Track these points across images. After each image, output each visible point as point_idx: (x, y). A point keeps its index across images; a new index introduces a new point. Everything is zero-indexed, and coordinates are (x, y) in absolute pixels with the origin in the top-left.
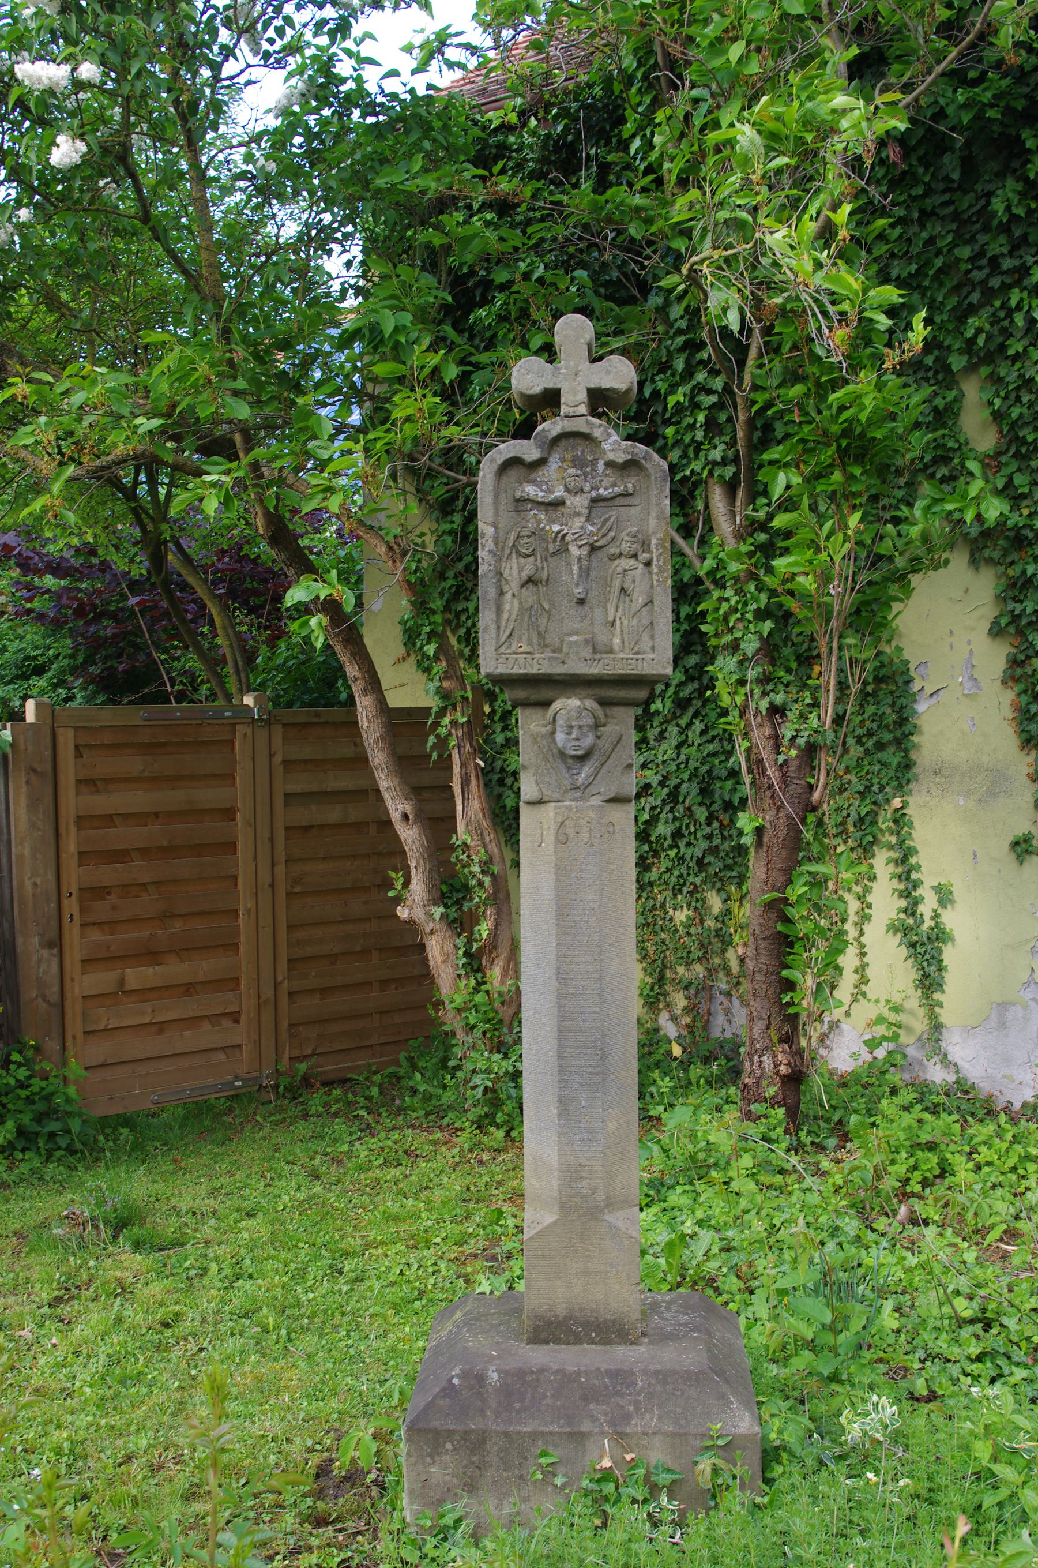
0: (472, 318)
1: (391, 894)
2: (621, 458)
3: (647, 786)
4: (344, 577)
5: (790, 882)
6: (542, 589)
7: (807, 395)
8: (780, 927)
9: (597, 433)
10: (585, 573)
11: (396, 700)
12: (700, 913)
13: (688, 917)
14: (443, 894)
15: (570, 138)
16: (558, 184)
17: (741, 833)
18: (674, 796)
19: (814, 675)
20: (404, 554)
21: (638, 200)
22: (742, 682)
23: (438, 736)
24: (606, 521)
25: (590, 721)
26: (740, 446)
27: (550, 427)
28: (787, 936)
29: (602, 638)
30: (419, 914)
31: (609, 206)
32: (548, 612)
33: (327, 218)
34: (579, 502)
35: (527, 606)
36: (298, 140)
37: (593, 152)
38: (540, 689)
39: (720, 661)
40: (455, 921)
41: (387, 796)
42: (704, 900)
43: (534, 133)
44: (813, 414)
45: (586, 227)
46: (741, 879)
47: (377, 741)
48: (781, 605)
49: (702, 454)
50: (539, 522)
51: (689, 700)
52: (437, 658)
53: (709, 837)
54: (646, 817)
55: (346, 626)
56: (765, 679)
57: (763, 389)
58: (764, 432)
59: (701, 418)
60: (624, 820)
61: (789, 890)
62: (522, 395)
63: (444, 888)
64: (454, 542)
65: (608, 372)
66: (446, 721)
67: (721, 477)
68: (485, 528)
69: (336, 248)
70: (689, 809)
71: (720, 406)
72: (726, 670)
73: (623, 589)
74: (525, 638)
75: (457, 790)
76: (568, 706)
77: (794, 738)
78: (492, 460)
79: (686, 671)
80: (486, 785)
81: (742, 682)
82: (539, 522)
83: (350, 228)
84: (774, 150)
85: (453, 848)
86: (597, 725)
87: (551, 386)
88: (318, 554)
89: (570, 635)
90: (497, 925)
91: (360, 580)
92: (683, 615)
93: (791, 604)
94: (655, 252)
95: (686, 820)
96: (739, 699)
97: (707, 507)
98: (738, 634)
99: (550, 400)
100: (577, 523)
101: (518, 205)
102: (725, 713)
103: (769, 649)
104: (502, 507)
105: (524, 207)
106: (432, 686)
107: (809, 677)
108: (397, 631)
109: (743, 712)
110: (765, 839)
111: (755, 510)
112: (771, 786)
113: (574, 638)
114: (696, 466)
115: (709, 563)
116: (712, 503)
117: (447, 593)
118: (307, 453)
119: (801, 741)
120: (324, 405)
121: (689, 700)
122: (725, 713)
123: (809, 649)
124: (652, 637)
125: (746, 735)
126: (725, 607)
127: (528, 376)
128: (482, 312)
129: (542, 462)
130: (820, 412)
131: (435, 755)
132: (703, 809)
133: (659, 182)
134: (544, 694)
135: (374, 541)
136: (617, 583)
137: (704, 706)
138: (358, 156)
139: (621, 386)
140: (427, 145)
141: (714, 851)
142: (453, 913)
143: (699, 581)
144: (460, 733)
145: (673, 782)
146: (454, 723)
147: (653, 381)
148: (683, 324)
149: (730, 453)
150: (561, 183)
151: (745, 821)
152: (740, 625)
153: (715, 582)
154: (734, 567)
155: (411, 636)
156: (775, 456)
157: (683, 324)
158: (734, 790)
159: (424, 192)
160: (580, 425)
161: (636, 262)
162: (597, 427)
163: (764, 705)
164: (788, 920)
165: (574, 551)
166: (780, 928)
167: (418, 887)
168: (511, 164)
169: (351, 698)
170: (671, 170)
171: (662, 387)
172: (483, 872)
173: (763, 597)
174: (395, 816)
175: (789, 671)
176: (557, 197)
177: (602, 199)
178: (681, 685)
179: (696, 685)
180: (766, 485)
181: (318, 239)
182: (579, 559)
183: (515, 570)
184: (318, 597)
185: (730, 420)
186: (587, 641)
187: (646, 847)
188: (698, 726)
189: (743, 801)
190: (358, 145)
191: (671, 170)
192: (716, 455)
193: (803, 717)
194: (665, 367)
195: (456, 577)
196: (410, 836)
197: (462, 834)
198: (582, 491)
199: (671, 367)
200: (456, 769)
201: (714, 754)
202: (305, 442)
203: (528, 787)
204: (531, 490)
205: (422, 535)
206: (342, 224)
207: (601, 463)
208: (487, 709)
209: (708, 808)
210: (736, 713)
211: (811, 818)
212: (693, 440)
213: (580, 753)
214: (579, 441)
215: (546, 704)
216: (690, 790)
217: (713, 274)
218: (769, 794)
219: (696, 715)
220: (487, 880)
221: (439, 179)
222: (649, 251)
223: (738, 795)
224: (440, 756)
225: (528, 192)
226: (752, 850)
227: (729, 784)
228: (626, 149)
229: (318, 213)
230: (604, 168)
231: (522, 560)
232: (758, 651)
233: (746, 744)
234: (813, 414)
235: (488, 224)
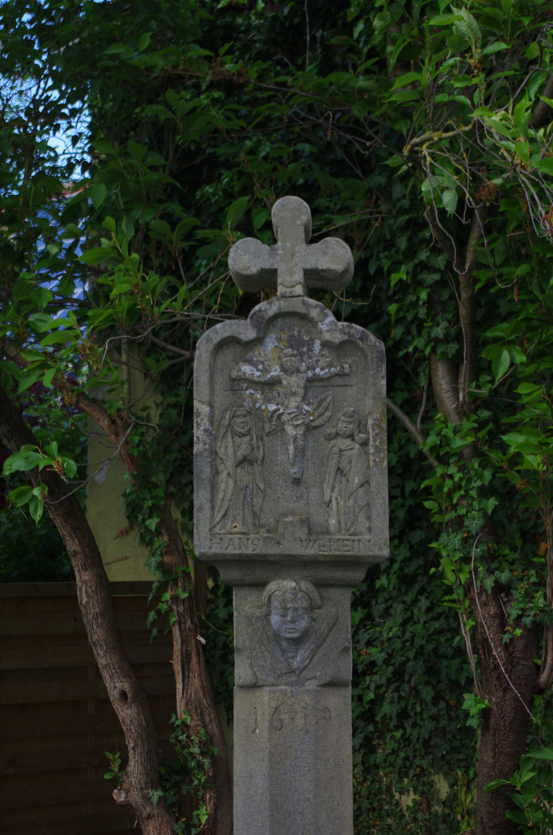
0: (198, 194)
1: (107, 776)
2: (337, 338)
3: (372, 664)
4: (65, 448)
5: (517, 767)
6: (257, 468)
7: (531, 274)
8: (508, 815)
9: (314, 313)
10: (301, 452)
11: (118, 573)
12: (427, 794)
13: (414, 801)
14: (161, 776)
15: (296, 20)
16: (284, 66)
17: (467, 715)
18: (399, 675)
19: (541, 552)
20: (126, 426)
21: (361, 82)
22: (466, 560)
23: (158, 612)
24: (322, 400)
25: (306, 604)
26: (463, 323)
27: (266, 308)
28: (516, 825)
29: (317, 519)
30: (136, 797)
31: (333, 87)
32: (264, 492)
33: (55, 95)
34: (294, 382)
35: (242, 485)
36: (27, 17)
37: (319, 34)
38: (261, 568)
39: (444, 537)
40: (173, 804)
41: (105, 674)
42: (431, 784)
43: (260, 15)
44: (536, 292)
45: (311, 108)
46: (468, 764)
47: (96, 617)
48: (506, 482)
49: (425, 331)
50: (255, 402)
51: (414, 577)
52: (158, 532)
53: (433, 718)
54: (371, 696)
55: (68, 498)
56: (490, 558)
57: (485, 267)
58: (488, 309)
59: (424, 295)
60: (341, 704)
61: (516, 775)
62: (239, 275)
63: (163, 770)
64: (179, 414)
65: (324, 253)
66: (167, 596)
67: (444, 354)
68: (201, 408)
69: (63, 123)
70: (415, 688)
71: (441, 284)
72: (450, 547)
73: (339, 470)
74: (239, 518)
75: (177, 668)
76: (282, 586)
77: (520, 617)
78: (209, 340)
79: (411, 547)
80: (207, 662)
81: (466, 560)
82: (255, 402)
83: (78, 105)
84: (494, 35)
85: (172, 728)
86: (311, 608)
87: (267, 266)
88: (44, 425)
89: (286, 515)
90: (216, 808)
91: (84, 451)
92: (407, 490)
93: (517, 481)
94: (377, 133)
95: (412, 700)
96: (463, 577)
97: (430, 384)
98: (462, 511)
99: (264, 283)
100: (293, 403)
101: (243, 86)
102: (449, 590)
103: (494, 526)
104: (217, 387)
105: (250, 87)
106: (153, 561)
107: (536, 555)
108: (120, 504)
109: (468, 589)
110: (492, 722)
111: (478, 387)
112: (497, 667)
113: (289, 519)
114: (419, 343)
115: (432, 440)
116: (434, 379)
117: (167, 470)
118: (28, 326)
119: (527, 621)
120: (48, 279)
121: (414, 577)
122: (449, 590)
123: (536, 526)
124: (369, 518)
125: (471, 614)
126: (448, 484)
127: (245, 257)
128: (209, 189)
129: (259, 341)
130: (543, 291)
131: (155, 632)
132: (429, 688)
133: (383, 64)
134: (259, 574)
135: (97, 414)
136: (333, 463)
137: (429, 582)
138: (85, 34)
139: (338, 267)
140: (153, 24)
141: (442, 732)
142: (171, 796)
143: (422, 456)
144: (181, 609)
145: (399, 660)
146: (175, 599)
147: (378, 258)
148: (406, 203)
149: (453, 331)
150: (286, 65)
151: (471, 704)
152: (464, 502)
153: (439, 459)
154: (458, 443)
155: (133, 510)
156: (499, 334)
157: (406, 203)
158: (460, 669)
159: (150, 69)
160: (297, 306)
161: (360, 143)
162: (314, 308)
163: (489, 583)
164: (516, 808)
165: (290, 430)
166: (508, 815)
167: (135, 767)
168: (238, 45)
169: (72, 571)
170: (393, 53)
171: (386, 264)
172: (203, 754)
173: (488, 474)
174: (114, 694)
175: (514, 549)
176: (282, 79)
177: (325, 81)
178: (406, 561)
179: (421, 561)
180: (490, 362)
181: (47, 115)
182: (295, 439)
183: (229, 450)
184: (37, 467)
185: (452, 297)
186: (302, 521)
187: (371, 728)
188: (424, 602)
189: (470, 681)
190: (86, 23)
191: (393, 53)
192: (439, 331)
193: (529, 596)
194: (389, 245)
195: (179, 451)
196: (127, 714)
197: (182, 713)
198: (298, 370)
199: (394, 245)
200: (177, 646)
201: (439, 632)
202: (27, 316)
203: (242, 672)
204: (247, 369)
205: (145, 408)
206: (71, 100)
207: (317, 343)
208: (210, 584)
209: (434, 687)
210: (461, 591)
211: (539, 701)
212: (416, 317)
213: (295, 635)
214: (295, 321)
215: (261, 585)
216: (416, 669)
217: (432, 155)
218: (494, 674)
219: (422, 591)
220: (207, 762)
221: (165, 56)
222: (370, 132)
223: (466, 674)
224: (160, 632)
225: (253, 73)
226: (479, 732)
227: (456, 663)
228: (351, 34)
229: (45, 91)
230: (328, 50)
231: (238, 439)
232: (483, 528)
233: (471, 623)
234: (536, 292)
235: (215, 101)
